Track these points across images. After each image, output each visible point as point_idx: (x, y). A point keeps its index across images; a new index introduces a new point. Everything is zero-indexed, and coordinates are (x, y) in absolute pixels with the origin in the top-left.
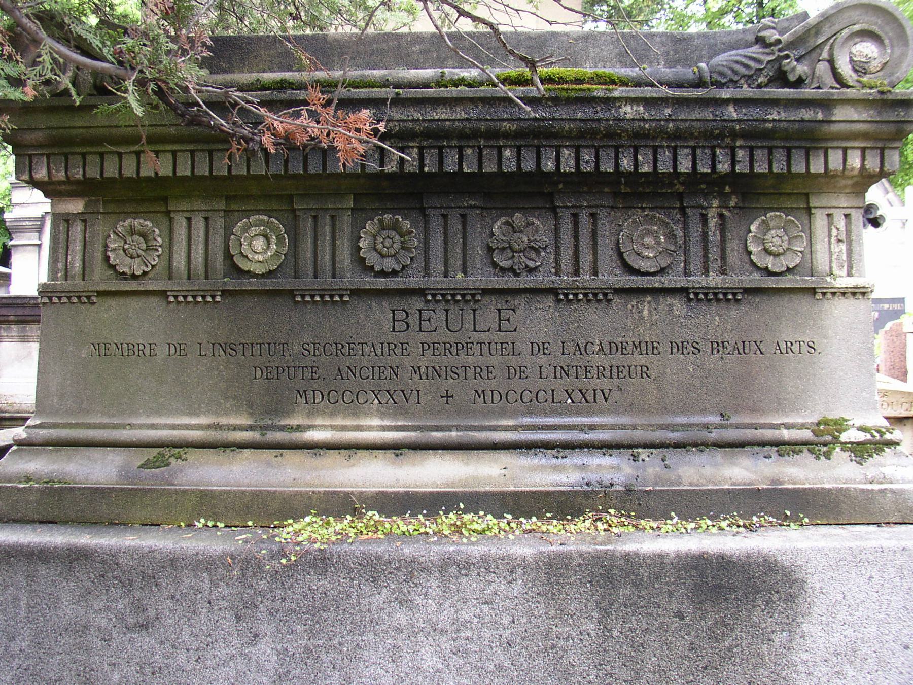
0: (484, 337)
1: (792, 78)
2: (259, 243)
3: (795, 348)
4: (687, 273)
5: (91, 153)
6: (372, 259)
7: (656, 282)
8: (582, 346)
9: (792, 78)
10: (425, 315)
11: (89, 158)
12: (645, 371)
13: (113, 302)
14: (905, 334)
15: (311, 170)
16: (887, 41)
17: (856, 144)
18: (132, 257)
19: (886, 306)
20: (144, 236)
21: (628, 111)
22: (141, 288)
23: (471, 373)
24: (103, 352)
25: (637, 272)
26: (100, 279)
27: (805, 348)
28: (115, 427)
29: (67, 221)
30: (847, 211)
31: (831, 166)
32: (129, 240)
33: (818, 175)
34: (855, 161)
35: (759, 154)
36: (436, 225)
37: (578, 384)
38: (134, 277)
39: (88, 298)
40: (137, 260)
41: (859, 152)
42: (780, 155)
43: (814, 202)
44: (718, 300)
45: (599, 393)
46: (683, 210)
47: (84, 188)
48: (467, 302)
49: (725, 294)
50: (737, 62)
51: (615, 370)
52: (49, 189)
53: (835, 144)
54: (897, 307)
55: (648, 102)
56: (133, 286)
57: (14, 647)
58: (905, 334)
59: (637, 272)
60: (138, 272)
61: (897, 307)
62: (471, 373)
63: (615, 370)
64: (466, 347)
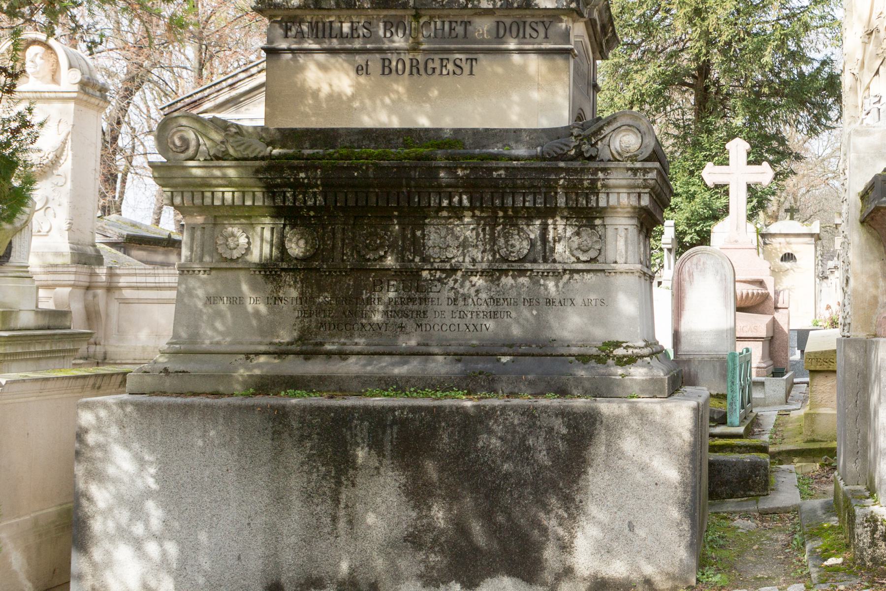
30: (626, 227)
38: (232, 260)
53: (613, 190)
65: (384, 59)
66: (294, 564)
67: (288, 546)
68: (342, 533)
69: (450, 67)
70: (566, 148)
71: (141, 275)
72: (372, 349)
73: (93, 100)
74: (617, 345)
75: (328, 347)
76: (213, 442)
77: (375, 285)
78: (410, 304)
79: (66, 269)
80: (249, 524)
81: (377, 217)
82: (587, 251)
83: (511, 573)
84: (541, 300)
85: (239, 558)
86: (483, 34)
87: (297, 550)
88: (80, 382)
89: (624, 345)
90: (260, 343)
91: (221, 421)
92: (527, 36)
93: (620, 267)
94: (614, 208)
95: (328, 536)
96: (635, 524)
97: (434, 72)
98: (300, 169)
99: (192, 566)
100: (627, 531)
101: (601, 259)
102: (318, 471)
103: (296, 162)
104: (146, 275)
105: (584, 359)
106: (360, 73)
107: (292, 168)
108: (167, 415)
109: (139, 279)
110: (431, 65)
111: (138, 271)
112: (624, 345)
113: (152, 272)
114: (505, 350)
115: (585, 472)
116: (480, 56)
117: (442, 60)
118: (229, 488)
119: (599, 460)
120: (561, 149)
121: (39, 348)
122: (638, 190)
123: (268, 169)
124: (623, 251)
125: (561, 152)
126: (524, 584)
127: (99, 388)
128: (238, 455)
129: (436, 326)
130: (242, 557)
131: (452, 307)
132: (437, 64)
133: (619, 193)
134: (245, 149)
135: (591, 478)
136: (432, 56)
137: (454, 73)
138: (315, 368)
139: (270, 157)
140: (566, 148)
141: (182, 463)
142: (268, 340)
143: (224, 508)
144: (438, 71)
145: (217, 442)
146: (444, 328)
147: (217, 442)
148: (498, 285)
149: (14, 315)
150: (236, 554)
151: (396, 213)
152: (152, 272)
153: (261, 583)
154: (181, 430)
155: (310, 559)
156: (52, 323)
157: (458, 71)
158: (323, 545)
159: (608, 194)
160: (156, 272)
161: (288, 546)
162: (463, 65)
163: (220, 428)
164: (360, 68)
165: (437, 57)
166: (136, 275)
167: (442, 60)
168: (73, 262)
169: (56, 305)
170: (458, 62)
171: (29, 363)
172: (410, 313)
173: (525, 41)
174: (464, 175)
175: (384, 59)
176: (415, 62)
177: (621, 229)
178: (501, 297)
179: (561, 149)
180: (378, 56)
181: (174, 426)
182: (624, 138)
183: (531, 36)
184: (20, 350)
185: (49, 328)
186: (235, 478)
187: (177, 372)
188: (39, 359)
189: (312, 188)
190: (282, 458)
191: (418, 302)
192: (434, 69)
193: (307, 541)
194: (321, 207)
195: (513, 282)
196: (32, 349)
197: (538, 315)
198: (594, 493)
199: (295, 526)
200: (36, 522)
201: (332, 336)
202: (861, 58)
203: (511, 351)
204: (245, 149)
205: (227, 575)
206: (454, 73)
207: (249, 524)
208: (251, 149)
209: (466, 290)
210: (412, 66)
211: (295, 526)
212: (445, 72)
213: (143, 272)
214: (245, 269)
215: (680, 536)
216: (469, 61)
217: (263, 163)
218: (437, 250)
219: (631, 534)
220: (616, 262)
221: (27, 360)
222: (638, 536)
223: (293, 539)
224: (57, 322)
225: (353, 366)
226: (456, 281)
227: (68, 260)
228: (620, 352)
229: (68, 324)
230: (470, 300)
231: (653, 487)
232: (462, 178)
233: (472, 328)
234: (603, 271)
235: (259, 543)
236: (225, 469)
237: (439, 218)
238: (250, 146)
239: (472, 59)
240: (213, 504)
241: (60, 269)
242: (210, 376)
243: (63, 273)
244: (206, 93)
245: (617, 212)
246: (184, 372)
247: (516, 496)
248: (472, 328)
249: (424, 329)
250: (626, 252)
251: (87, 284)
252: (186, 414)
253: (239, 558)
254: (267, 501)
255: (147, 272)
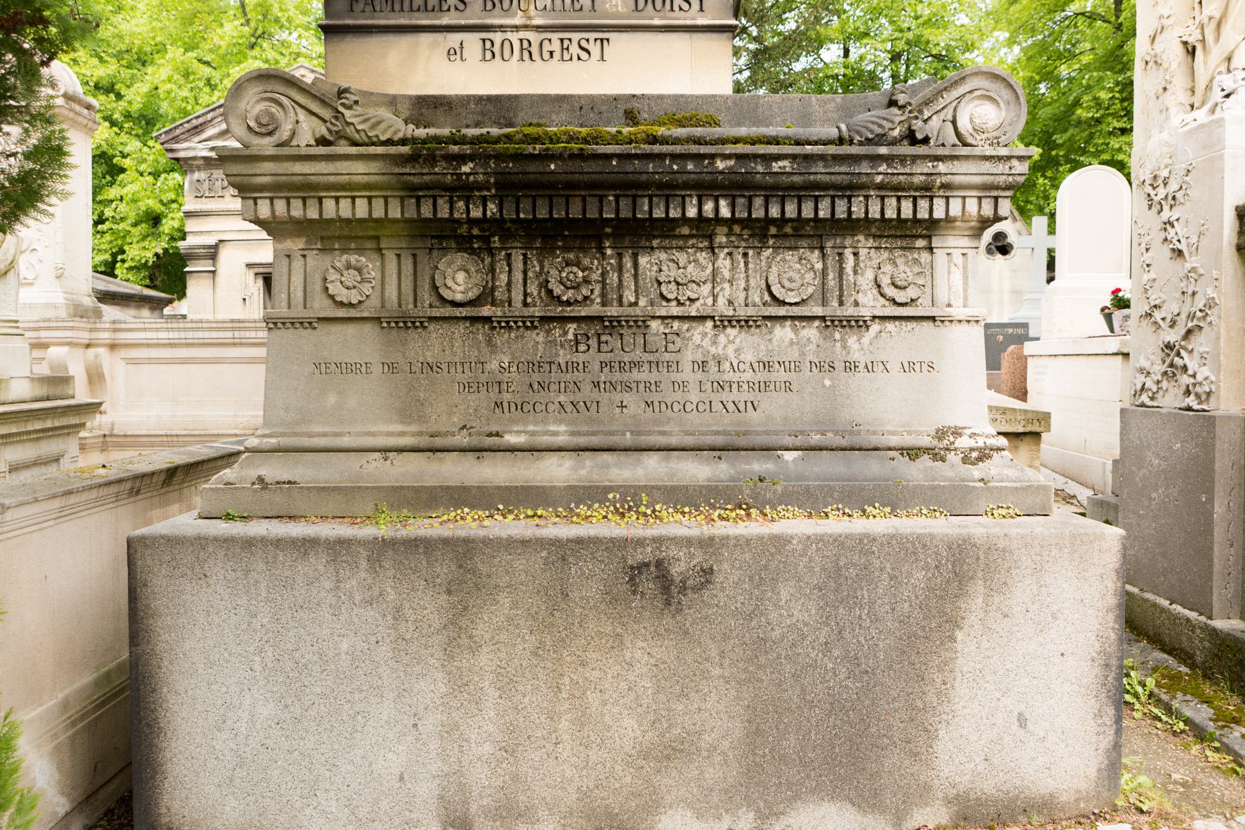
0: (651, 357)
1: (919, 136)
2: (461, 276)
3: (917, 367)
4: (824, 303)
5: (376, 197)
6: (558, 290)
7: (796, 311)
8: (735, 365)
9: (919, 136)
10: (603, 338)
11: (309, 202)
12: (788, 386)
13: (337, 328)
14: (1026, 357)
15: (821, 214)
16: (1002, 105)
17: (364, 194)
18: (348, 288)
19: (1010, 331)
20: (359, 270)
21: (720, 165)
22: (358, 315)
23: (642, 386)
24: (323, 370)
25: (784, 303)
26: (321, 307)
27: (925, 367)
28: (337, 435)
29: (289, 256)
30: (964, 251)
31: (952, 213)
32: (345, 273)
33: (939, 220)
34: (972, 206)
35: (623, 203)
36: (390, 256)
37: (732, 397)
38: (351, 305)
39: (310, 323)
40: (354, 291)
41: (382, 201)
42: (526, 204)
43: (936, 242)
44: (851, 327)
45: (749, 405)
46: (822, 248)
47: (301, 227)
48: (639, 327)
49: (849, 321)
50: (873, 123)
51: (762, 384)
52: (272, 227)
53: (956, 193)
54: (1020, 331)
55: (740, 157)
56: (353, 313)
57: (256, 623)
58: (1026, 357)
59: (784, 303)
60: (354, 301)
61: (1020, 331)
62: (642, 386)
63: (762, 384)
64: (636, 364)
65: (484, 40)
66: (490, 786)
67: (479, 759)
68: (566, 737)
69: (574, 50)
70: (887, 125)
71: (150, 330)
72: (582, 441)
73: (80, 119)
74: (957, 433)
75: (511, 439)
76: (351, 597)
77: (577, 343)
78: (635, 371)
79: (60, 324)
80: (415, 725)
81: (576, 236)
82: (905, 288)
83: (834, 794)
84: (836, 365)
85: (401, 778)
86: (616, 6)
87: (493, 765)
88: (114, 489)
89: (968, 432)
90: (402, 434)
91: (364, 564)
92: (676, 8)
93: (958, 312)
94: (954, 220)
95: (544, 743)
96: (1028, 717)
97: (552, 56)
98: (462, 159)
99: (327, 790)
100: (1015, 727)
101: (925, 301)
102: (525, 641)
103: (455, 149)
104: (157, 330)
105: (913, 453)
106: (452, 58)
107: (450, 158)
108: (275, 557)
109: (149, 335)
110: (547, 47)
111: (147, 326)
112: (968, 432)
113: (165, 325)
114: (788, 441)
115: (953, 639)
116: (612, 36)
117: (562, 40)
118: (380, 671)
119: (972, 619)
120: (880, 126)
121: (38, 425)
122: (995, 193)
123: (412, 159)
124: (961, 288)
125: (879, 131)
126: (853, 810)
127: (138, 492)
128: (395, 619)
129: (675, 404)
130: (406, 777)
131: (700, 375)
132: (556, 46)
133: (964, 198)
134: (373, 127)
135: (959, 646)
136: (549, 35)
137: (579, 58)
138: (495, 472)
139: (414, 141)
140: (887, 125)
141: (302, 632)
142: (414, 428)
143: (373, 700)
144: (557, 55)
145: (358, 598)
146: (688, 408)
147: (358, 598)
148: (770, 340)
149: (4, 385)
150: (397, 772)
151: (608, 230)
152: (165, 325)
153: (438, 815)
154: (299, 579)
155: (515, 778)
156: (52, 391)
157: (584, 55)
158: (536, 756)
159: (947, 198)
160: (170, 326)
161: (479, 759)
162: (590, 47)
163: (363, 575)
164: (452, 52)
165: (555, 37)
166: (145, 330)
167: (562, 40)
168: (69, 315)
169: (51, 369)
170: (584, 44)
171: (27, 445)
172: (634, 385)
173: (672, 14)
174: (726, 168)
175: (484, 40)
176: (526, 44)
177: (957, 254)
178: (776, 359)
179: (880, 126)
180: (478, 36)
181: (288, 573)
182: (978, 109)
183: (681, 9)
184: (14, 430)
185: (48, 399)
186: (390, 655)
187: (278, 483)
188: (38, 439)
189: (480, 189)
190: (464, 622)
191: (646, 366)
192: (551, 53)
193: (510, 751)
194: (493, 221)
195: (792, 336)
196: (30, 428)
197: (833, 386)
198: (965, 669)
199: (491, 728)
200: (65, 705)
201: (513, 421)
202: (1217, 15)
203: (798, 441)
204: (373, 127)
205: (384, 804)
206: (579, 58)
207: (415, 725)
208: (383, 126)
209: (720, 349)
210: (522, 49)
211: (491, 728)
212: (566, 57)
213: (154, 326)
214: (372, 319)
215: (1098, 734)
216: (599, 42)
217: (405, 149)
218: (673, 286)
219: (1022, 731)
220: (949, 305)
221: (23, 441)
222: (1032, 734)
223: (487, 748)
224: (58, 391)
225: (557, 471)
226: (704, 335)
227: (63, 313)
228: (964, 442)
229: (71, 392)
230: (728, 364)
231: (1057, 659)
232: (721, 173)
233: (731, 407)
234: (933, 319)
235: (433, 755)
236: (373, 639)
237: (675, 237)
238: (379, 123)
239: (602, 40)
240: (357, 696)
241: (54, 324)
242: (334, 489)
243: (57, 328)
244: (209, 116)
245: (954, 228)
246: (290, 482)
247: (842, 677)
248: (731, 407)
249: (657, 409)
250: (965, 290)
251: (87, 342)
252: (306, 554)
253: (401, 778)
254: (444, 690)
255: (159, 326)
